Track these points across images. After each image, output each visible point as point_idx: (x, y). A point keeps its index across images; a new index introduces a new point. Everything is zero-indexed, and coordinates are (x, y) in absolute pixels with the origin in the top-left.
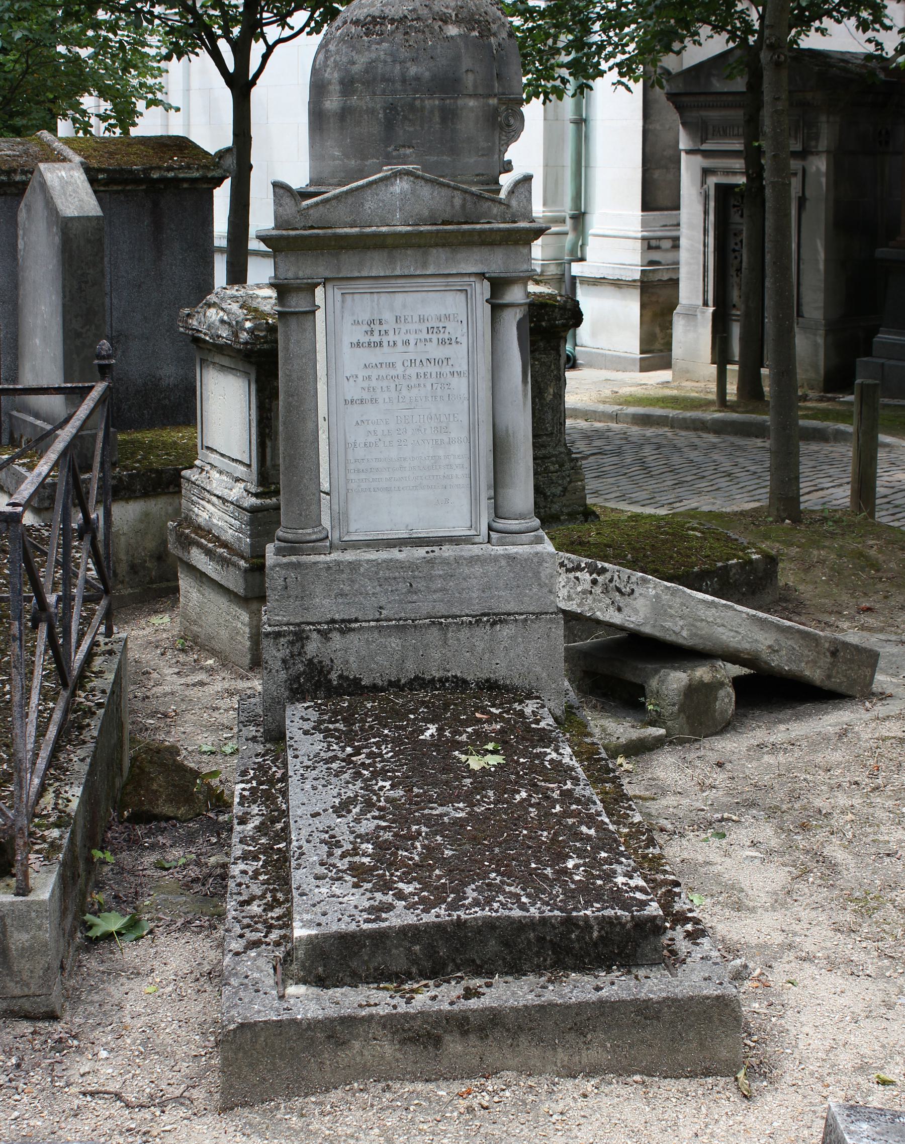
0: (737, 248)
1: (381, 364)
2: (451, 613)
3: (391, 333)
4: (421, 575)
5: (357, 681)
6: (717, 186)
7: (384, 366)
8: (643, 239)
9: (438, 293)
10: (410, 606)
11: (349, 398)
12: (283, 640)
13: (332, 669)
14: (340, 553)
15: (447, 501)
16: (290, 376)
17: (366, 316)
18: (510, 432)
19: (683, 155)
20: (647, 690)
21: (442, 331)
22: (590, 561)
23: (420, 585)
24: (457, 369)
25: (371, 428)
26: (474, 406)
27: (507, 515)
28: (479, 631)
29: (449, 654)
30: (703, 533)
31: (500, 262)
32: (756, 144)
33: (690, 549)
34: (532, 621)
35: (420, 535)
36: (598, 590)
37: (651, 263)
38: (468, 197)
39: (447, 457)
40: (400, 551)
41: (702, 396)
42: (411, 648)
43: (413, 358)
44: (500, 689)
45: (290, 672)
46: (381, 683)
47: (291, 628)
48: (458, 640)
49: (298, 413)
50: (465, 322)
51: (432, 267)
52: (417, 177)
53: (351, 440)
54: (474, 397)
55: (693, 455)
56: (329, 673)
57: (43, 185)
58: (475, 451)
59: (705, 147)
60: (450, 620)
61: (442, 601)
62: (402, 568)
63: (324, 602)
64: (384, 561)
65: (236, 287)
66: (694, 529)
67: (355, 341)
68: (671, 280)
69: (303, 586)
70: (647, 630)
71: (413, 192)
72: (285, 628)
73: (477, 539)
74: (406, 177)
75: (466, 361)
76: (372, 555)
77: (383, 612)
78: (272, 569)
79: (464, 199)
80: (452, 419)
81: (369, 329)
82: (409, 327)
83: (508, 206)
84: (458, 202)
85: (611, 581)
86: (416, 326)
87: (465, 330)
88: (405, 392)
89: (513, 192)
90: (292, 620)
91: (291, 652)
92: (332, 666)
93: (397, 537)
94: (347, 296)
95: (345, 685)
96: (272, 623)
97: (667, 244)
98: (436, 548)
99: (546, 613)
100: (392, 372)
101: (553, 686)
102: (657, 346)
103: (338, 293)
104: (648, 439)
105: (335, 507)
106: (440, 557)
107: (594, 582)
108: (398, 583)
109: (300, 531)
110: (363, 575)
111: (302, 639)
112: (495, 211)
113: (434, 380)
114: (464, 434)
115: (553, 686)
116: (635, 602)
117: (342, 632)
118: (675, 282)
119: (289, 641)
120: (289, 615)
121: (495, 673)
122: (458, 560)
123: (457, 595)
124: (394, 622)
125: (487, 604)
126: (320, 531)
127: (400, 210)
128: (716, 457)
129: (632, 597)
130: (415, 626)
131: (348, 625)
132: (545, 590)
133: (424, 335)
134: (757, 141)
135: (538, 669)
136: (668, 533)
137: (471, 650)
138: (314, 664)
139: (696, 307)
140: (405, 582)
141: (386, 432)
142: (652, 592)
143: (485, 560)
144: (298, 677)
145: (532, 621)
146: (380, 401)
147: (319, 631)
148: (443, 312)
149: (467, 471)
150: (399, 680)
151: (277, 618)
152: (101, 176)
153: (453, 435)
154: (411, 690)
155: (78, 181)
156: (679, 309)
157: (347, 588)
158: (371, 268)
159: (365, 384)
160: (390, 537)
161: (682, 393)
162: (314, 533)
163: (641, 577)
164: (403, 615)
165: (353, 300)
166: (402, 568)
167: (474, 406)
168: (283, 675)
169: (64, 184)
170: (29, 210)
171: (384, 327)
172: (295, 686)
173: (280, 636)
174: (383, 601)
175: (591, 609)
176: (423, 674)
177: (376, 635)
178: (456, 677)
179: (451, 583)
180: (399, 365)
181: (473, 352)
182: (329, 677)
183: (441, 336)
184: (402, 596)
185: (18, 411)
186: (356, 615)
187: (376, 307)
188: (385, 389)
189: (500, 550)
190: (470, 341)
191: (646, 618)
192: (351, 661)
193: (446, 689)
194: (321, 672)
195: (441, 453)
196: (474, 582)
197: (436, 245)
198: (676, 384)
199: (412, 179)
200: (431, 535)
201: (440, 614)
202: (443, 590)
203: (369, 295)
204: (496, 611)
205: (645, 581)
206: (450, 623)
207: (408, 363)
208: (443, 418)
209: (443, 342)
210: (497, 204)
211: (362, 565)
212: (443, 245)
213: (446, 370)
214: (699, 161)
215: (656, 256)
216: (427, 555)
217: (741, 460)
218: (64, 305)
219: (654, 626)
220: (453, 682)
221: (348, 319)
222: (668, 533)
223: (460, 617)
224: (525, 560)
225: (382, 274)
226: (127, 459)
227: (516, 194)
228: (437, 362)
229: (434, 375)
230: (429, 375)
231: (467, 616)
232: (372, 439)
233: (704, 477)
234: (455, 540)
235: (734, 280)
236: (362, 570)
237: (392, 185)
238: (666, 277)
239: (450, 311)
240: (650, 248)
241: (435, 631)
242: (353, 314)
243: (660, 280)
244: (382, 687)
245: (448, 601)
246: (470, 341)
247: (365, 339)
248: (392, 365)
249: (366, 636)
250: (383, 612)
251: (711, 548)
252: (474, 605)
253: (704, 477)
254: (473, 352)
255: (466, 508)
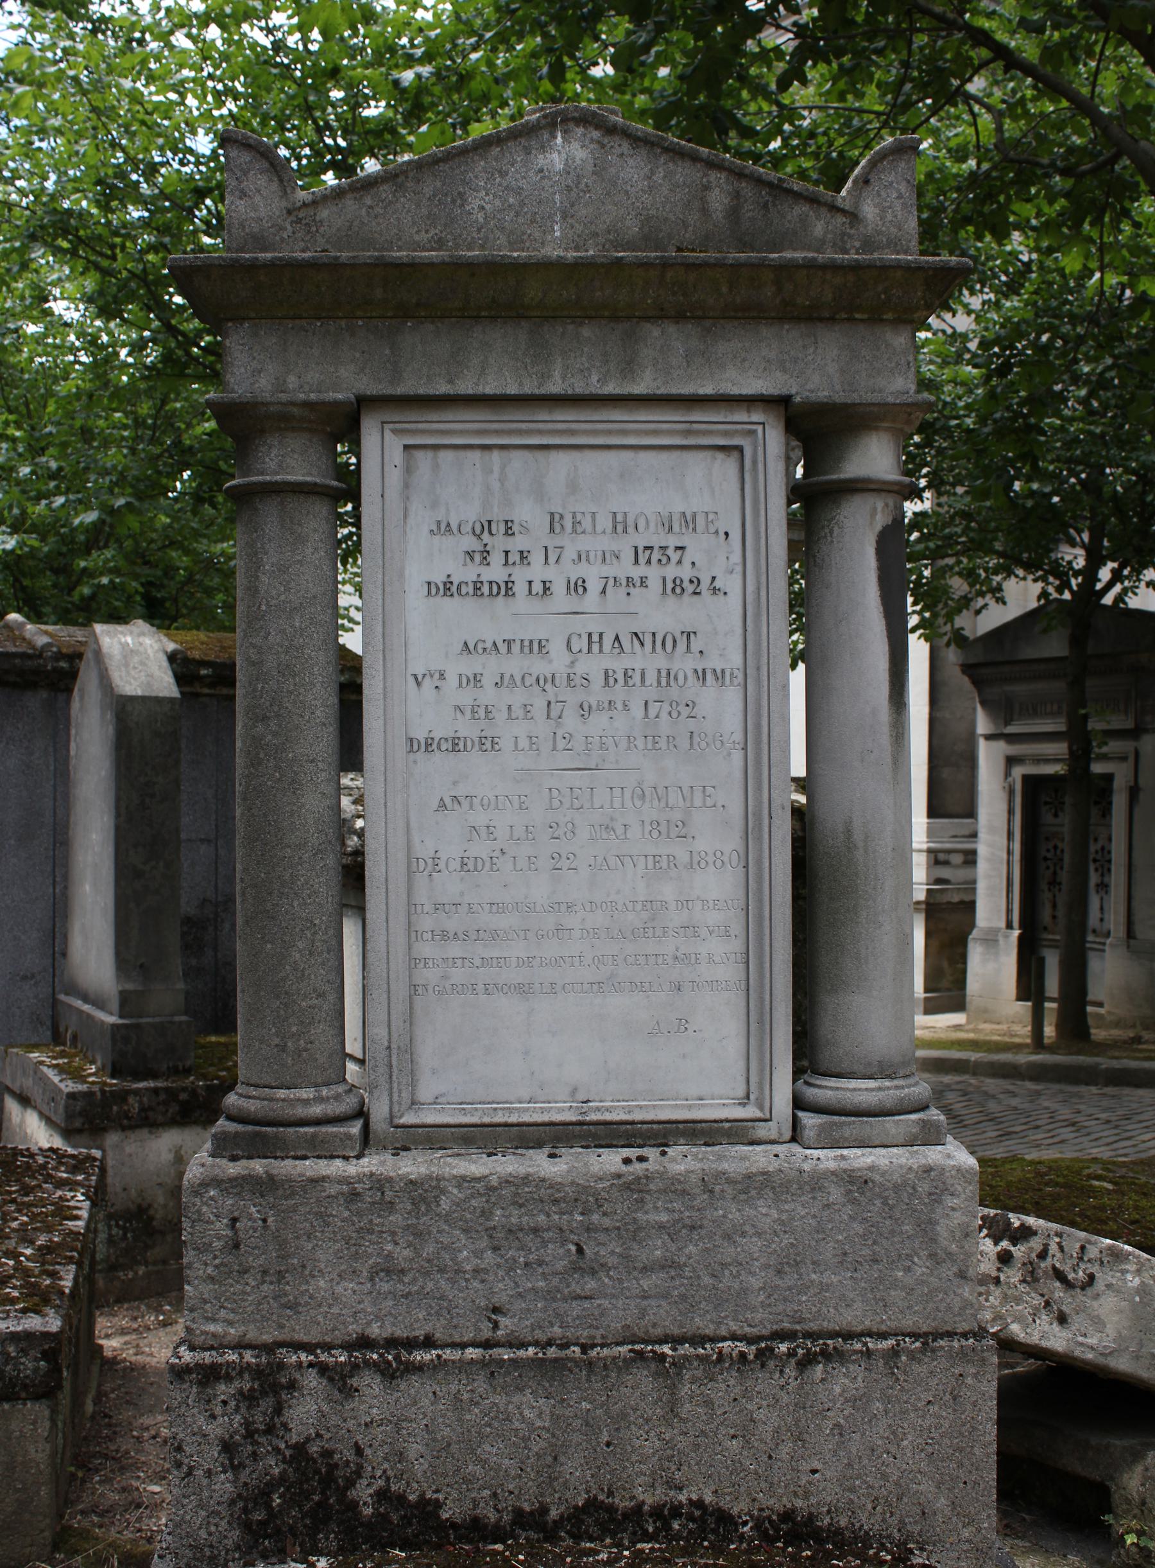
0: (1049, 855)
1: (509, 643)
2: (689, 1329)
3: (537, 558)
4: (607, 1222)
5: (427, 1509)
6: (1026, 779)
7: (516, 648)
8: (929, 851)
9: (664, 456)
10: (576, 1308)
11: (420, 735)
12: (223, 1390)
13: (358, 1474)
14: (388, 1156)
15: (683, 1024)
16: (261, 663)
17: (469, 512)
18: (858, 836)
19: (982, 744)
20: (1116, 1498)
21: (675, 558)
22: (992, 1212)
23: (606, 1250)
24: (714, 662)
25: (480, 818)
26: (758, 763)
27: (845, 1066)
28: (765, 1382)
29: (682, 1443)
30: (1115, 1183)
31: (832, 368)
32: (1083, 711)
33: (1102, 1208)
34: (912, 1356)
35: (608, 1117)
36: (1013, 1275)
37: (938, 881)
38: (746, 188)
39: (684, 904)
40: (552, 1156)
41: (1007, 1039)
42: (577, 1423)
43: (595, 629)
44: (820, 1541)
45: (244, 1477)
46: (493, 1517)
47: (249, 1357)
48: (708, 1403)
49: (278, 768)
50: (735, 536)
51: (648, 374)
52: (611, 130)
53: (424, 850)
54: (758, 742)
55: (1014, 1102)
56: (351, 1483)
57: (98, 653)
58: (760, 890)
59: (1010, 729)
60: (686, 1349)
61: (666, 1296)
62: (556, 1201)
63: (339, 1289)
64: (507, 1181)
65: (351, 776)
66: (1099, 1178)
67: (439, 579)
68: (962, 902)
69: (282, 1244)
70: (1122, 1364)
71: (599, 169)
72: (232, 1357)
73: (762, 1131)
74: (580, 131)
75: (739, 641)
76: (476, 1165)
77: (503, 1321)
78: (196, 1193)
79: (737, 195)
80: (698, 802)
81: (476, 545)
82: (585, 543)
83: (853, 217)
84: (718, 200)
85: (1043, 1255)
86: (606, 543)
87: (736, 557)
88: (571, 721)
89: (867, 182)
90: (252, 1335)
91: (247, 1424)
92: (360, 1467)
93: (545, 1118)
94: (419, 455)
95: (395, 1518)
96: (199, 1340)
97: (957, 859)
98: (652, 1153)
99: (950, 1335)
100: (539, 667)
101: (966, 1533)
102: (945, 983)
103: (395, 445)
104: (948, 1085)
105: (379, 1032)
106: (662, 1175)
107: (1005, 1258)
108: (544, 1243)
109: (282, 1093)
110: (447, 1218)
111: (275, 1389)
112: (818, 229)
113: (651, 693)
114: (732, 843)
115: (966, 1533)
116: (1095, 1304)
117: (389, 1374)
118: (970, 907)
119: (240, 1392)
120: (244, 1322)
121: (807, 1495)
122: (709, 1184)
123: (707, 1280)
124: (531, 1350)
125: (790, 1308)
126: (337, 1098)
127: (564, 217)
128: (1046, 1104)
129: (1089, 1291)
130: (590, 1364)
131: (404, 1356)
132: (948, 1271)
133: (626, 568)
134: (1084, 707)
135: (926, 1487)
136: (1057, 1184)
137: (745, 1432)
138: (310, 1459)
139: (998, 930)
140: (564, 1242)
141: (519, 832)
142: (1133, 1281)
143: (786, 1186)
144: (264, 1495)
145: (912, 1356)
146: (506, 744)
147: (323, 1369)
148: (679, 507)
149: (737, 945)
150: (544, 1510)
151: (212, 1328)
152: (203, 672)
153: (701, 845)
154: (577, 1537)
155: (150, 651)
156: (975, 933)
157: (403, 1254)
158: (482, 373)
159: (466, 698)
160: (526, 1118)
161: (981, 1037)
162: (320, 1100)
163: (1110, 1248)
164: (557, 1330)
165: (436, 467)
166: (556, 1201)
167: (758, 763)
168: (224, 1485)
169: (128, 653)
170: (82, 698)
171: (518, 543)
172: (258, 1516)
173: (218, 1378)
174: (502, 1292)
175: (998, 1317)
176: (610, 1494)
177: (481, 1384)
178: (699, 1504)
179: (691, 1248)
180: (557, 647)
181: (757, 615)
182: (352, 1494)
183: (671, 572)
184: (555, 1281)
185: (67, 994)
186: (428, 1328)
187: (496, 485)
188: (518, 712)
189: (827, 1159)
190: (750, 588)
191: (1119, 1338)
192: (412, 1455)
193: (672, 1537)
194: (328, 1480)
195: (668, 892)
196: (755, 1245)
197: (660, 315)
198: (971, 1026)
199: (596, 134)
200: (638, 1116)
201: (658, 1332)
202: (668, 1265)
203: (476, 455)
204: (813, 1326)
205: (1117, 1256)
206: (686, 1358)
207: (580, 644)
208: (674, 798)
209: (676, 588)
210: (824, 211)
211: (443, 1191)
212: (679, 317)
213: (685, 664)
214: (1001, 748)
215: (944, 873)
216: (624, 1168)
217: (1082, 1107)
218: (117, 828)
219: (1137, 1358)
220: (691, 1518)
221: (421, 519)
222: (1057, 1184)
223: (714, 1340)
224: (897, 1188)
225: (512, 390)
226: (211, 1065)
227: (875, 186)
228: (662, 642)
229: (651, 678)
230: (637, 678)
231: (734, 1337)
232: (480, 849)
233: (1037, 1127)
234: (703, 1132)
235: (1046, 896)
236: (445, 1204)
237: (543, 148)
238: (956, 899)
239: (698, 503)
240: (937, 862)
241: (643, 1379)
242: (435, 505)
243: (949, 903)
244: (497, 1525)
245: (683, 1297)
246: (750, 588)
247: (467, 573)
248: (539, 647)
249: (453, 1388)
250: (503, 1321)
251: (1136, 1208)
252: (753, 1309)
253: (1037, 1127)
254: (757, 615)
255: (734, 1047)
